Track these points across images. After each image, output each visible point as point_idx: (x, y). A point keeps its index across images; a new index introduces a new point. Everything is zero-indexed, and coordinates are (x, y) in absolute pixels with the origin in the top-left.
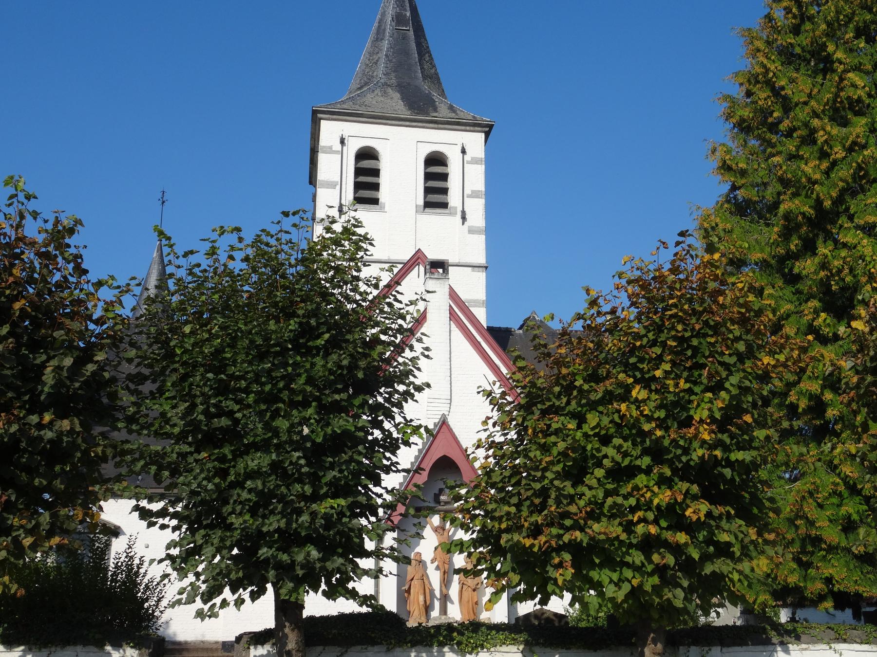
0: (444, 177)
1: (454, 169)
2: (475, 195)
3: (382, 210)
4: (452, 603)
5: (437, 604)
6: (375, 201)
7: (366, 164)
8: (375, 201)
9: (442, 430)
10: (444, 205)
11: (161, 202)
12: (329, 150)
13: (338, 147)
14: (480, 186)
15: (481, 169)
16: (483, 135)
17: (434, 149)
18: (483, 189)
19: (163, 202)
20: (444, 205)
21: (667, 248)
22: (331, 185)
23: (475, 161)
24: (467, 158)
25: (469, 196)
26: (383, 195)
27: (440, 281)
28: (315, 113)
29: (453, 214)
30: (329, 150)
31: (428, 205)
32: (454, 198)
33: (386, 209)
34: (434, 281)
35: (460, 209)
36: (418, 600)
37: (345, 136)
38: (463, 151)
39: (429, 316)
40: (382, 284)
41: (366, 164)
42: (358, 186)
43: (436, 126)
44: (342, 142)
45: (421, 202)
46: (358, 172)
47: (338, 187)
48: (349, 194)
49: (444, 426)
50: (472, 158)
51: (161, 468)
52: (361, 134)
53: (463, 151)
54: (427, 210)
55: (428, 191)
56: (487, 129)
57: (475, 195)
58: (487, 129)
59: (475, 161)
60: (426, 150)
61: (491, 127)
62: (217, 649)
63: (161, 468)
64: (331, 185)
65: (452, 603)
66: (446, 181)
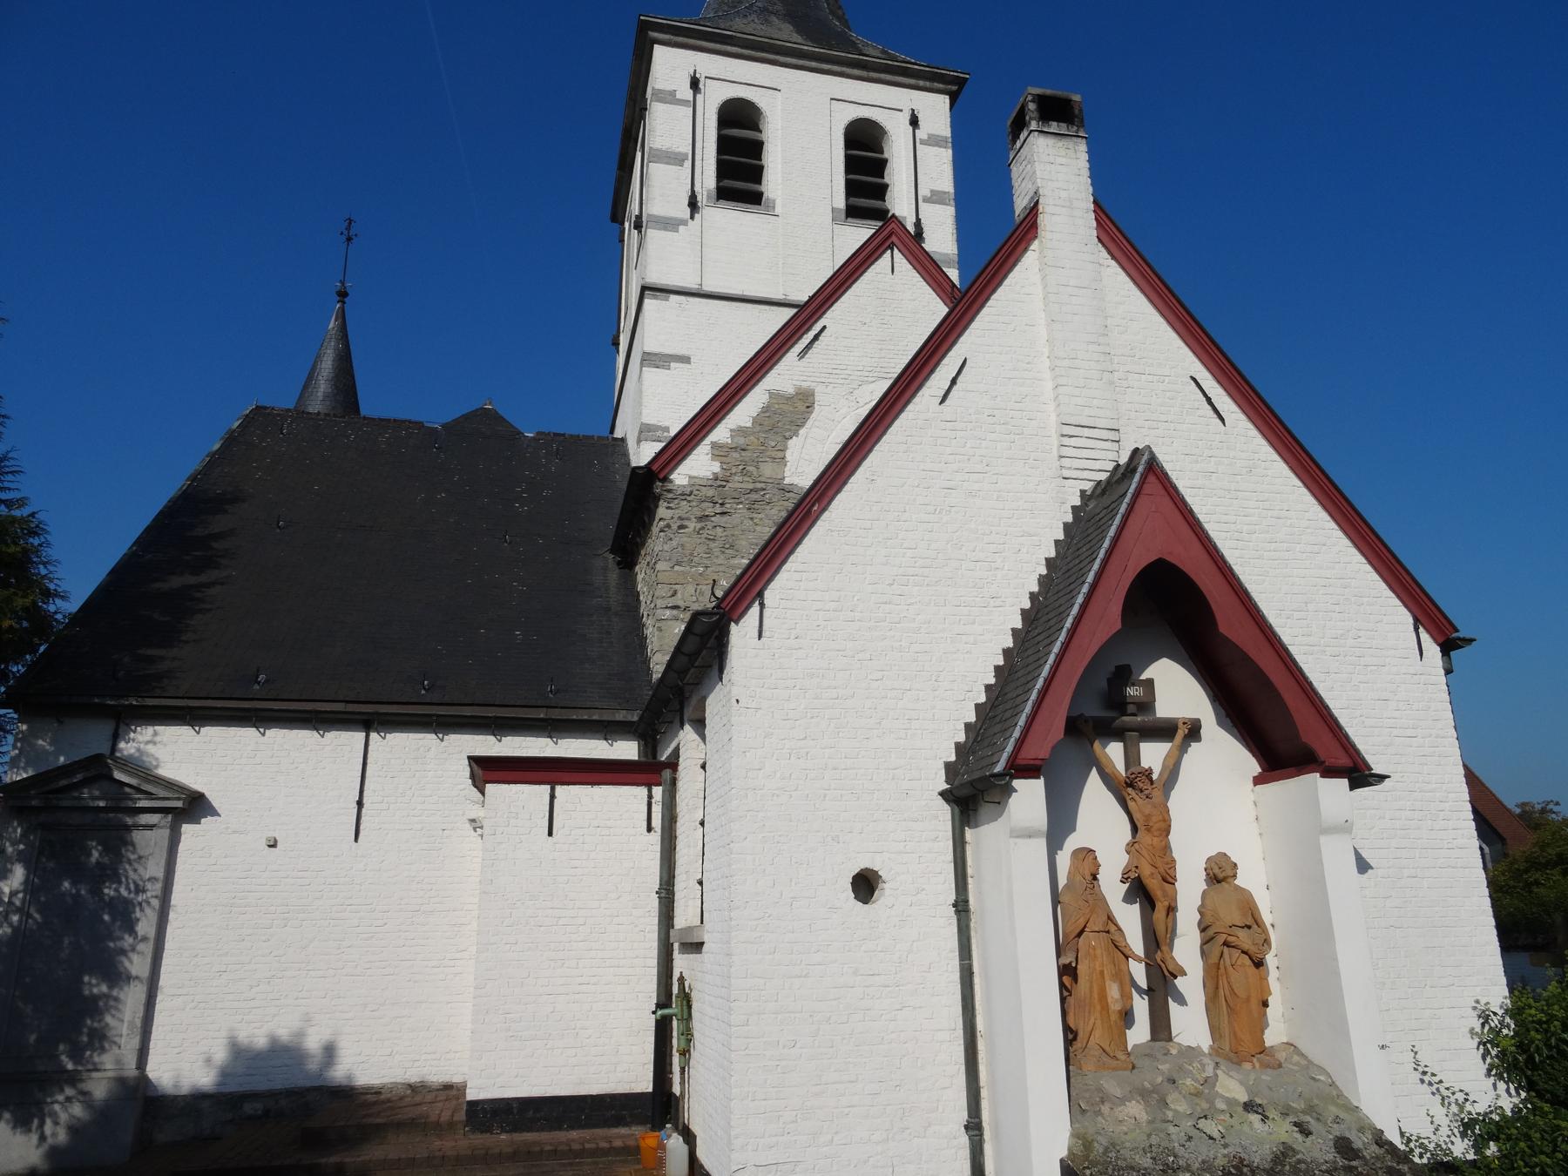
1: (898, 150)
2: (936, 198)
3: (770, 210)
4: (1181, 1001)
5: (1141, 1006)
9: (1147, 488)
11: (344, 238)
12: (670, 98)
13: (686, 93)
14: (946, 184)
15: (946, 154)
16: (946, 99)
18: (951, 190)
19: (349, 239)
22: (675, 159)
23: (933, 141)
24: (921, 134)
25: (926, 200)
27: (1062, 143)
28: (644, 27)
30: (670, 98)
33: (778, 210)
34: (1050, 141)
36: (1103, 996)
37: (701, 75)
38: (914, 122)
39: (1043, 220)
42: (723, 170)
43: (864, 73)
44: (695, 84)
45: (840, 202)
46: (724, 145)
47: (688, 164)
49: (1151, 478)
50: (930, 136)
52: (731, 76)
53: (914, 122)
56: (955, 88)
57: (936, 198)
58: (955, 88)
59: (933, 141)
61: (961, 83)
62: (451, 1125)
64: (675, 159)
65: (1181, 1001)
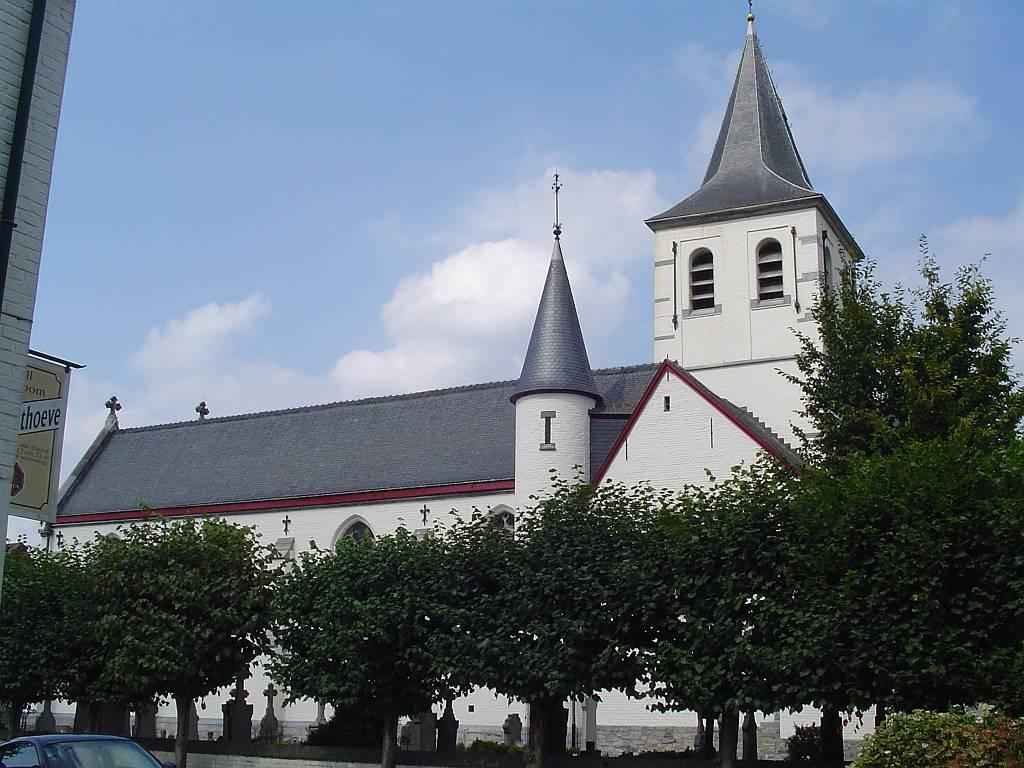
0: (778, 266)
2: (807, 277)
6: (709, 303)
7: (772, 259)
8: (709, 303)
10: (780, 295)
17: (765, 237)
20: (780, 295)
21: (530, 497)
23: (805, 240)
26: (718, 297)
29: (788, 301)
31: (763, 297)
32: (788, 287)
35: (794, 298)
38: (794, 232)
40: (820, 347)
41: (772, 259)
45: (755, 296)
48: (685, 301)
51: (614, 550)
53: (794, 232)
54: (763, 302)
55: (763, 283)
60: (757, 239)
63: (614, 550)
66: (781, 269)
